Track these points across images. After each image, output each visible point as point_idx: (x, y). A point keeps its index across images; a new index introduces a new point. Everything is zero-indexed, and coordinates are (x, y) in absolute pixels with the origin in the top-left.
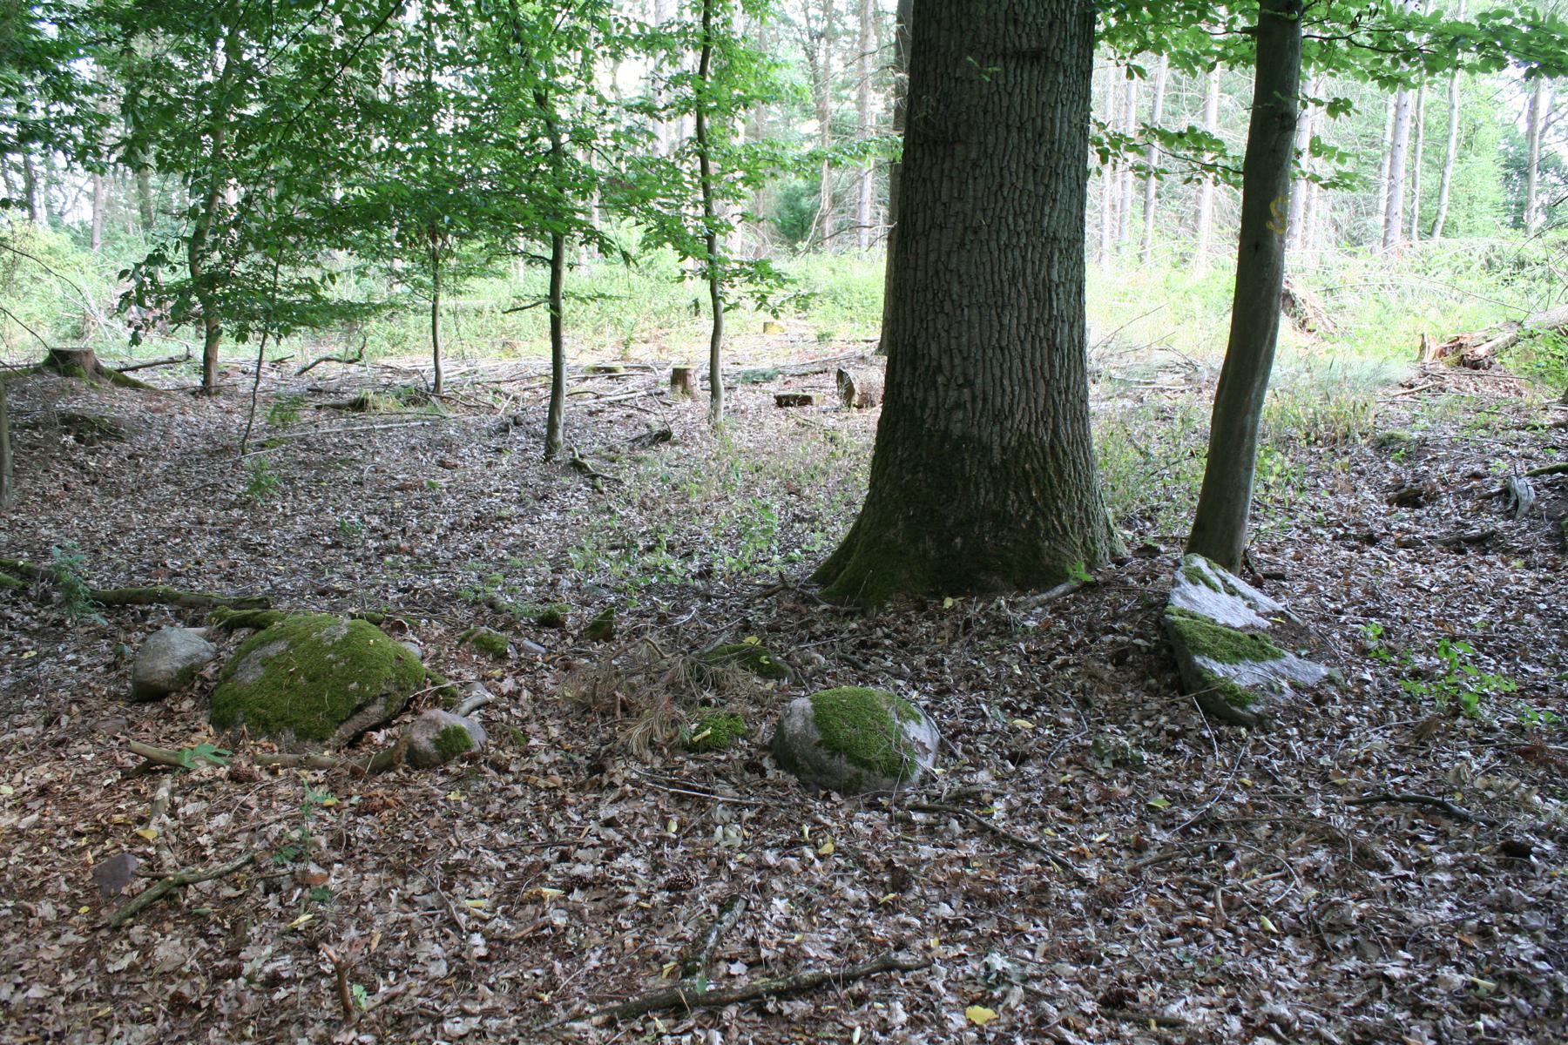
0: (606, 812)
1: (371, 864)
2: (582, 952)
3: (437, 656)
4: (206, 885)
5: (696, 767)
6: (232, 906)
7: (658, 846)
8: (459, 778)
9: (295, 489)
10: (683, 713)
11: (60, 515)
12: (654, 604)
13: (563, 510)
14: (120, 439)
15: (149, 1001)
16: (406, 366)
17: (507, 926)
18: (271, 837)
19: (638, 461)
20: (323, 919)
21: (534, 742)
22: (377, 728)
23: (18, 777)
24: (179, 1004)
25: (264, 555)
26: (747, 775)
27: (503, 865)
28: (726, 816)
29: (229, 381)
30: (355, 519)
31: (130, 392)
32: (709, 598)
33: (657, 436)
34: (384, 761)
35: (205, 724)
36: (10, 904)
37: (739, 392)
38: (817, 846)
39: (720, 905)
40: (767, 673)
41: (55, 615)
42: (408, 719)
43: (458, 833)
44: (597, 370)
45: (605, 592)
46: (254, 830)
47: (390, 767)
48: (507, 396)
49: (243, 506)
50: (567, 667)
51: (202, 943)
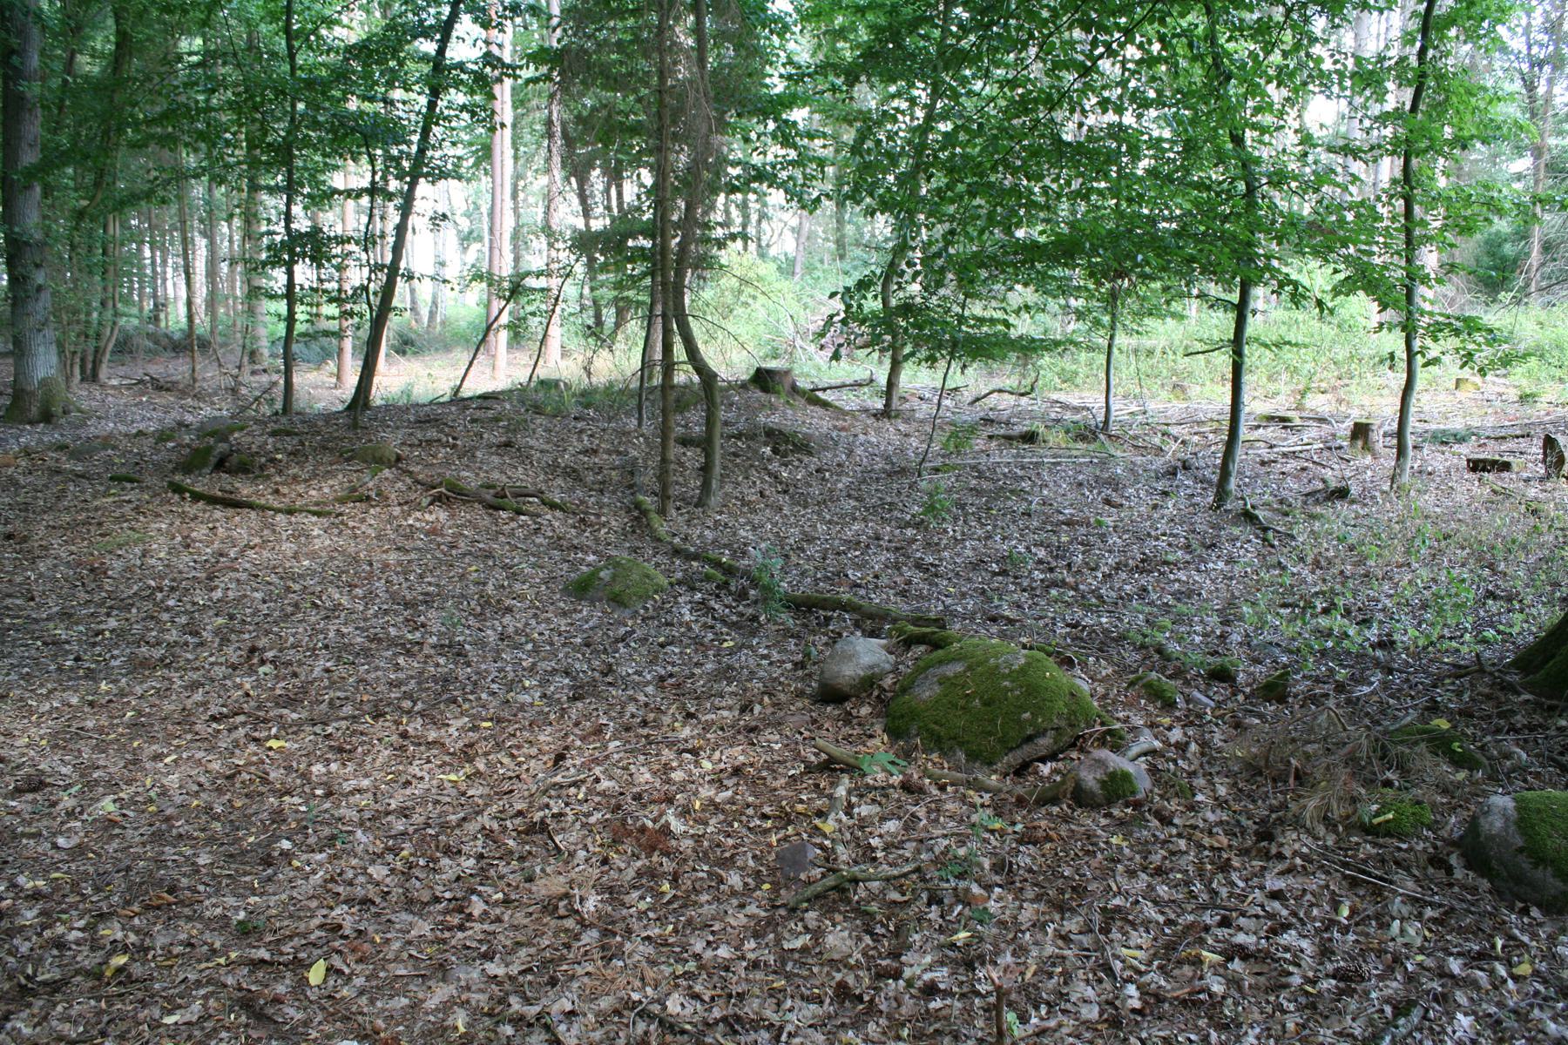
0: (1274, 883)
1: (1030, 894)
2: (1239, 1026)
3: (1105, 696)
4: (875, 885)
5: (1374, 851)
6: (897, 910)
7: (1327, 929)
8: (1121, 823)
9: (966, 515)
10: (1363, 791)
11: (756, 519)
12: (1331, 670)
13: (1231, 561)
14: (810, 454)
15: (818, 983)
16: (1076, 402)
17: (1163, 983)
18: (937, 850)
19: (1313, 517)
20: (981, 940)
21: (1200, 797)
22: (1043, 760)
23: (717, 754)
24: (843, 992)
25: (936, 575)
26: (1431, 870)
27: (1161, 919)
28: (1405, 910)
29: (907, 406)
30: (1021, 549)
31: (819, 410)
32: (1390, 671)
33: (1333, 493)
34: (1050, 794)
35: (880, 732)
36: (706, 868)
37: (1425, 451)
38: (1509, 965)
39: (1395, 1008)
40: (1459, 761)
41: (750, 611)
42: (1074, 755)
43: (1119, 879)
44: (1270, 418)
45: (1277, 651)
46: (921, 841)
47: (1055, 801)
48: (1176, 440)
49: (917, 526)
50: (1237, 725)
51: (868, 940)
